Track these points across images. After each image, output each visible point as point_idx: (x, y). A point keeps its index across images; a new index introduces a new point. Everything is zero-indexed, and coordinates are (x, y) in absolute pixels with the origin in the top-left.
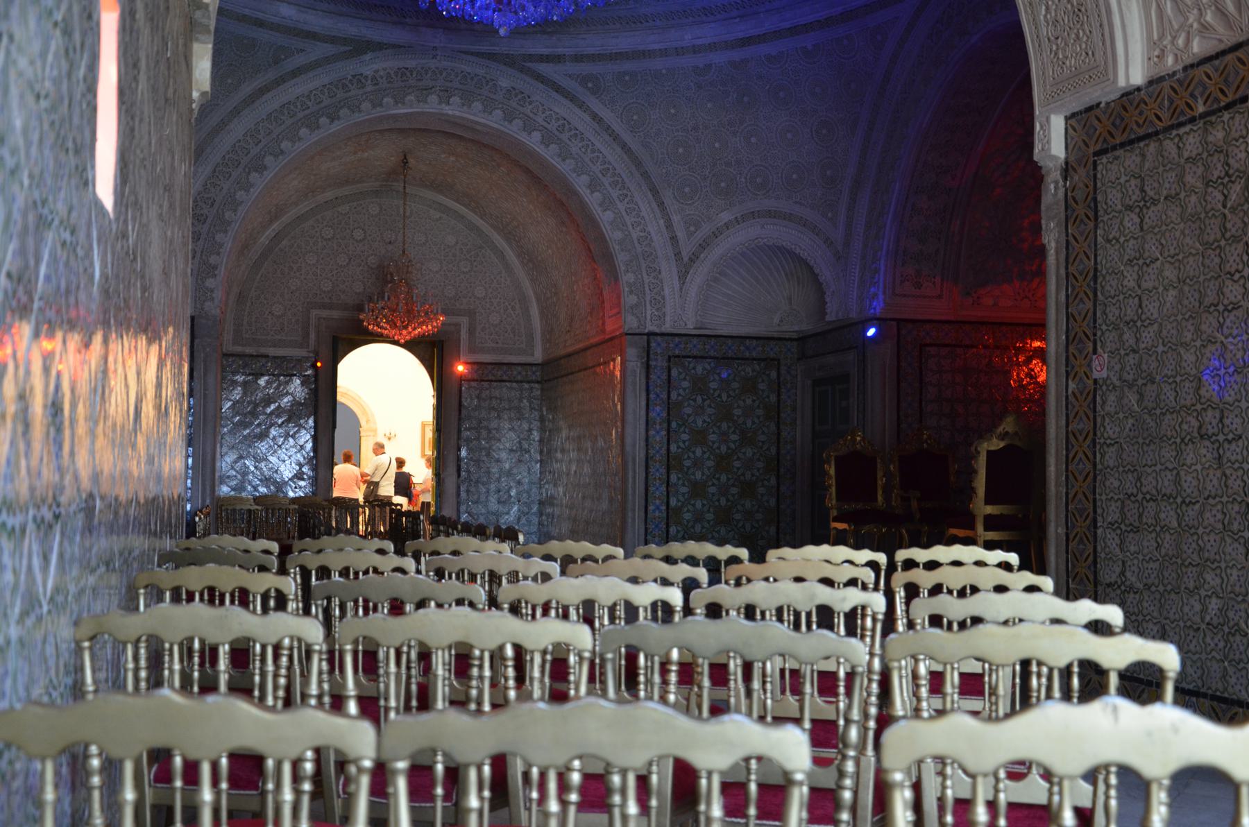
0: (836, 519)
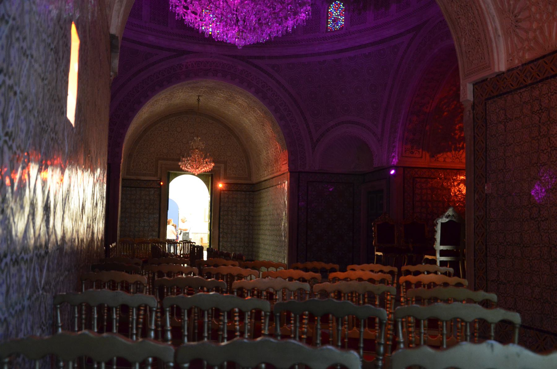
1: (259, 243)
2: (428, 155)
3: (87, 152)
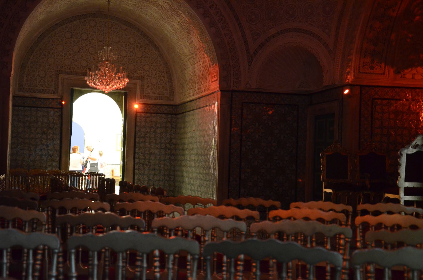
0: (326, 188)
1: (183, 176)
2: (392, 71)
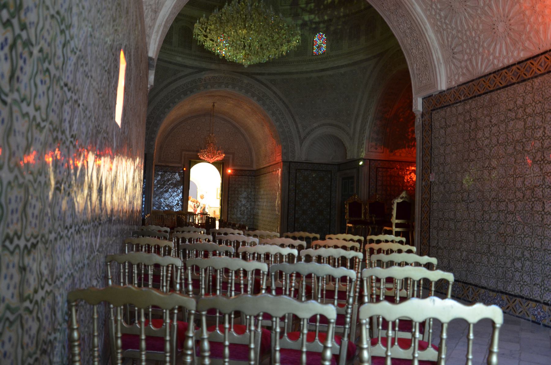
0: (348, 223)
3: (130, 146)
